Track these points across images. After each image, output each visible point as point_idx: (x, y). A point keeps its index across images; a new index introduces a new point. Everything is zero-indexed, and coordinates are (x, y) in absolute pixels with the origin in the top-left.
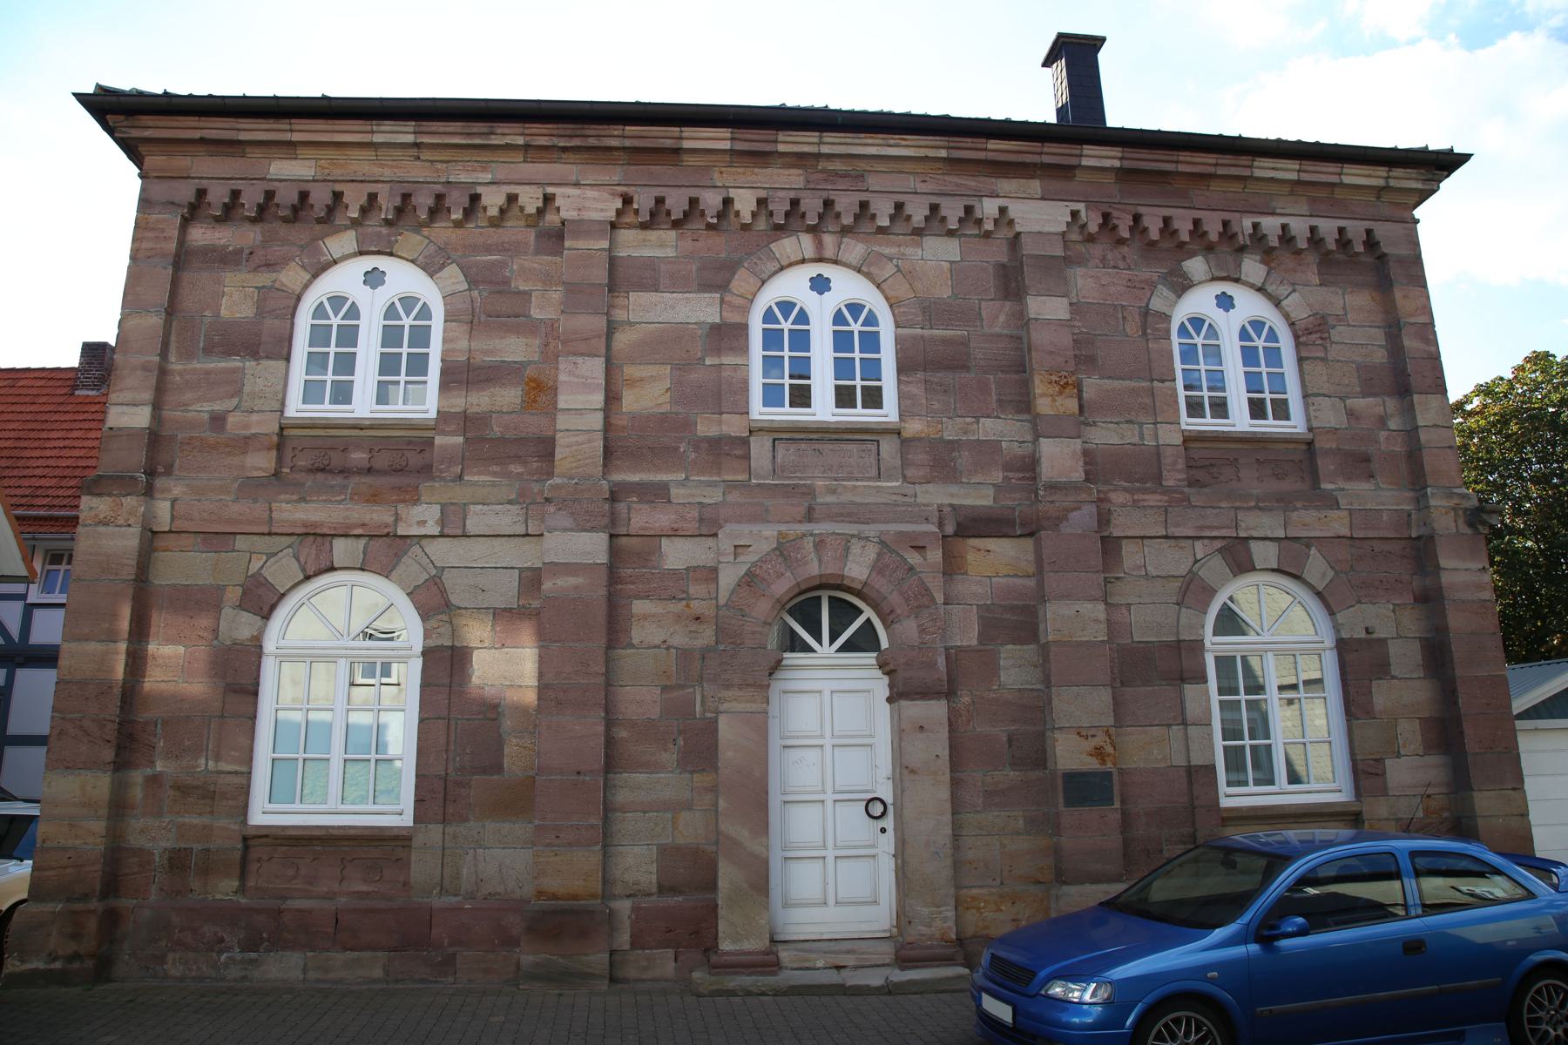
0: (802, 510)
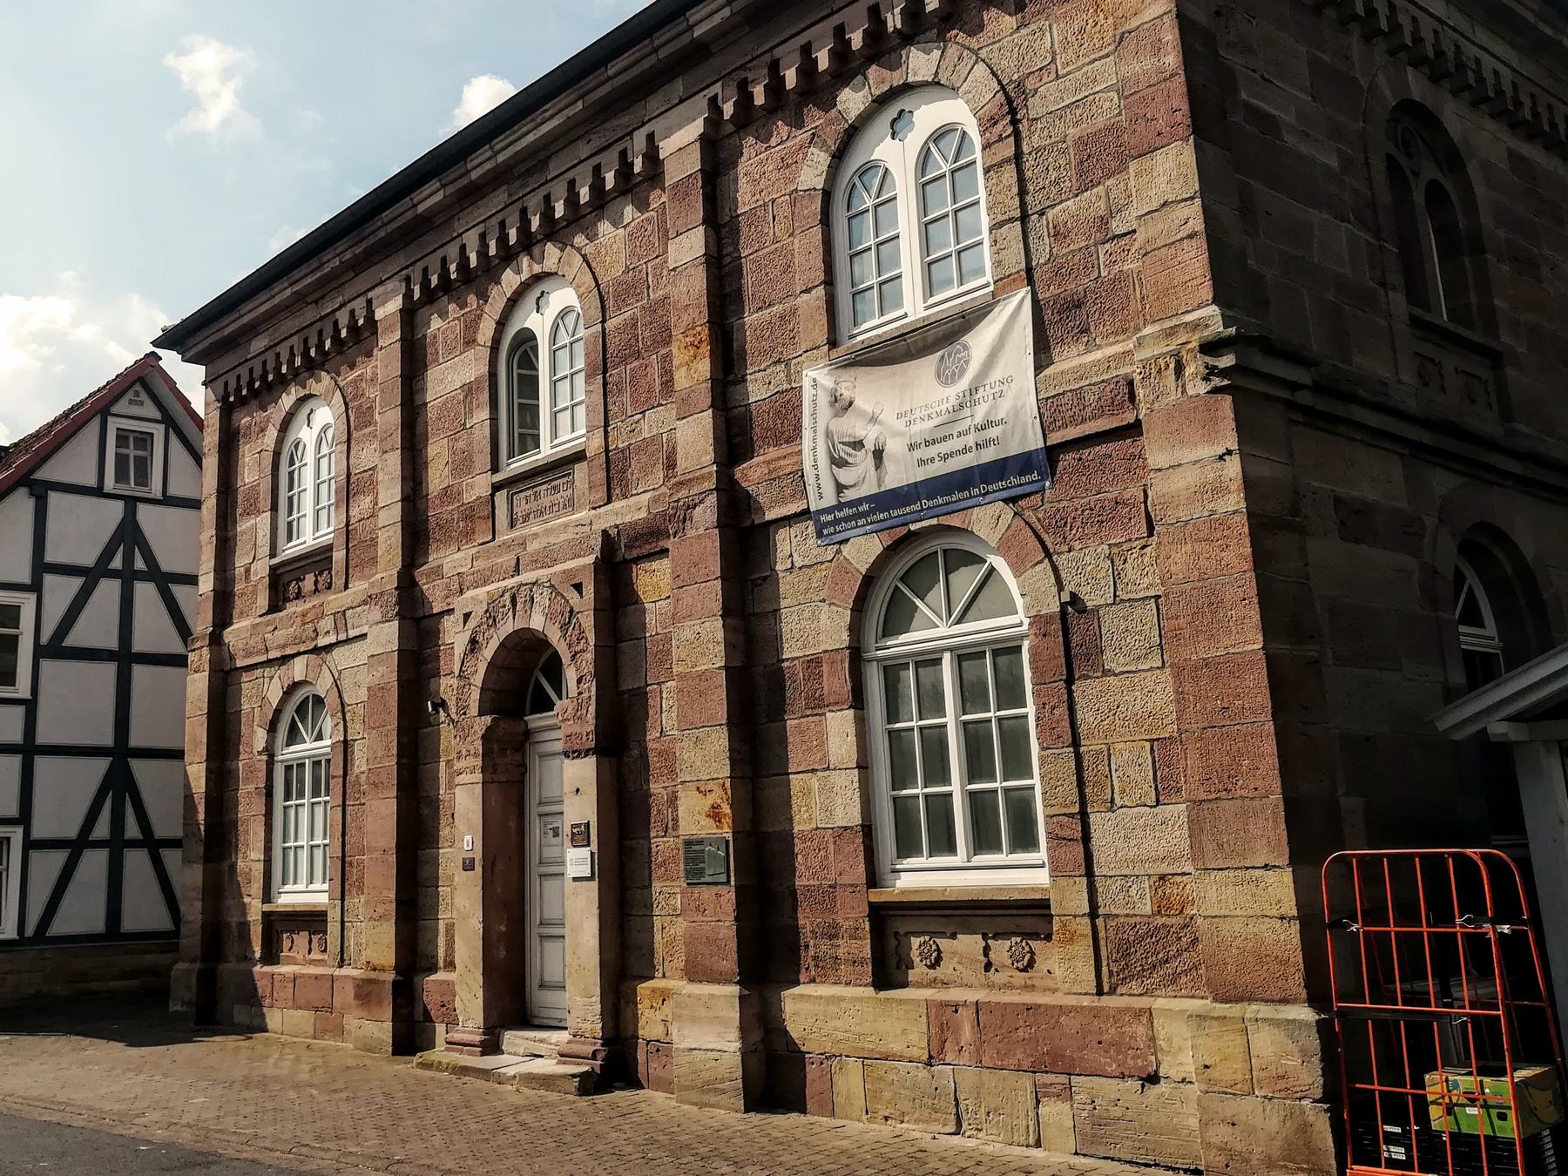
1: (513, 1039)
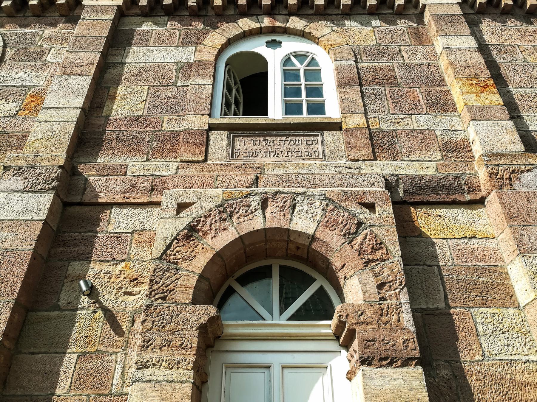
0: (252, 178)
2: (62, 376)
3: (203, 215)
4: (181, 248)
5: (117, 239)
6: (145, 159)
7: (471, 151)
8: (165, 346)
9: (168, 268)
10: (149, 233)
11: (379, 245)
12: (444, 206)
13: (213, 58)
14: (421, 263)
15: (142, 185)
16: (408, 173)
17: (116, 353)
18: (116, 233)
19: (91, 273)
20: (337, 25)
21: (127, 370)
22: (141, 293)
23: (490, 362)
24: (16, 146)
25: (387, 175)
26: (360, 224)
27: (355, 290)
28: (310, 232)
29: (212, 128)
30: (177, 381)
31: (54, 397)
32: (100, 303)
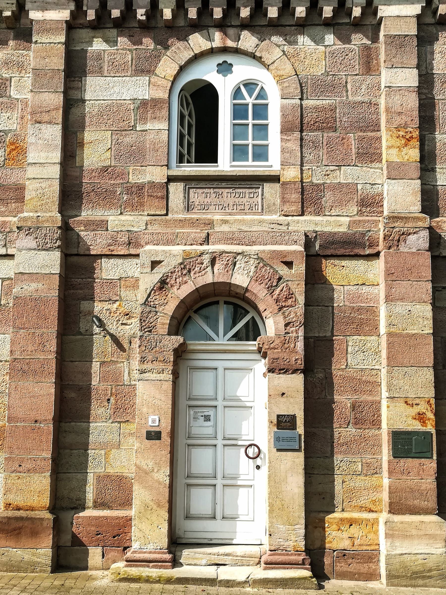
0: (204, 235)
1: (186, 554)
2: (93, 375)
3: (170, 271)
4: (157, 297)
5: (110, 284)
6: (119, 212)
7: (383, 205)
8: (154, 361)
9: (151, 311)
10: (132, 280)
11: (290, 295)
12: (348, 258)
13: (167, 96)
14: (321, 304)
15: (121, 240)
16: (325, 230)
17: (123, 362)
18: (109, 279)
19: (97, 310)
20: (290, 43)
21: (131, 372)
22: (133, 324)
23: (350, 370)
24: (14, 199)
25: (308, 231)
26: (280, 279)
27: (272, 326)
28: (245, 285)
29: (171, 179)
30: (163, 380)
31: (92, 386)
32: (107, 331)
